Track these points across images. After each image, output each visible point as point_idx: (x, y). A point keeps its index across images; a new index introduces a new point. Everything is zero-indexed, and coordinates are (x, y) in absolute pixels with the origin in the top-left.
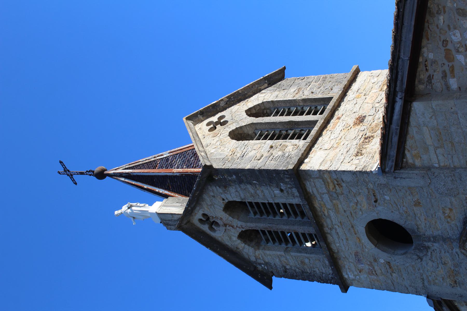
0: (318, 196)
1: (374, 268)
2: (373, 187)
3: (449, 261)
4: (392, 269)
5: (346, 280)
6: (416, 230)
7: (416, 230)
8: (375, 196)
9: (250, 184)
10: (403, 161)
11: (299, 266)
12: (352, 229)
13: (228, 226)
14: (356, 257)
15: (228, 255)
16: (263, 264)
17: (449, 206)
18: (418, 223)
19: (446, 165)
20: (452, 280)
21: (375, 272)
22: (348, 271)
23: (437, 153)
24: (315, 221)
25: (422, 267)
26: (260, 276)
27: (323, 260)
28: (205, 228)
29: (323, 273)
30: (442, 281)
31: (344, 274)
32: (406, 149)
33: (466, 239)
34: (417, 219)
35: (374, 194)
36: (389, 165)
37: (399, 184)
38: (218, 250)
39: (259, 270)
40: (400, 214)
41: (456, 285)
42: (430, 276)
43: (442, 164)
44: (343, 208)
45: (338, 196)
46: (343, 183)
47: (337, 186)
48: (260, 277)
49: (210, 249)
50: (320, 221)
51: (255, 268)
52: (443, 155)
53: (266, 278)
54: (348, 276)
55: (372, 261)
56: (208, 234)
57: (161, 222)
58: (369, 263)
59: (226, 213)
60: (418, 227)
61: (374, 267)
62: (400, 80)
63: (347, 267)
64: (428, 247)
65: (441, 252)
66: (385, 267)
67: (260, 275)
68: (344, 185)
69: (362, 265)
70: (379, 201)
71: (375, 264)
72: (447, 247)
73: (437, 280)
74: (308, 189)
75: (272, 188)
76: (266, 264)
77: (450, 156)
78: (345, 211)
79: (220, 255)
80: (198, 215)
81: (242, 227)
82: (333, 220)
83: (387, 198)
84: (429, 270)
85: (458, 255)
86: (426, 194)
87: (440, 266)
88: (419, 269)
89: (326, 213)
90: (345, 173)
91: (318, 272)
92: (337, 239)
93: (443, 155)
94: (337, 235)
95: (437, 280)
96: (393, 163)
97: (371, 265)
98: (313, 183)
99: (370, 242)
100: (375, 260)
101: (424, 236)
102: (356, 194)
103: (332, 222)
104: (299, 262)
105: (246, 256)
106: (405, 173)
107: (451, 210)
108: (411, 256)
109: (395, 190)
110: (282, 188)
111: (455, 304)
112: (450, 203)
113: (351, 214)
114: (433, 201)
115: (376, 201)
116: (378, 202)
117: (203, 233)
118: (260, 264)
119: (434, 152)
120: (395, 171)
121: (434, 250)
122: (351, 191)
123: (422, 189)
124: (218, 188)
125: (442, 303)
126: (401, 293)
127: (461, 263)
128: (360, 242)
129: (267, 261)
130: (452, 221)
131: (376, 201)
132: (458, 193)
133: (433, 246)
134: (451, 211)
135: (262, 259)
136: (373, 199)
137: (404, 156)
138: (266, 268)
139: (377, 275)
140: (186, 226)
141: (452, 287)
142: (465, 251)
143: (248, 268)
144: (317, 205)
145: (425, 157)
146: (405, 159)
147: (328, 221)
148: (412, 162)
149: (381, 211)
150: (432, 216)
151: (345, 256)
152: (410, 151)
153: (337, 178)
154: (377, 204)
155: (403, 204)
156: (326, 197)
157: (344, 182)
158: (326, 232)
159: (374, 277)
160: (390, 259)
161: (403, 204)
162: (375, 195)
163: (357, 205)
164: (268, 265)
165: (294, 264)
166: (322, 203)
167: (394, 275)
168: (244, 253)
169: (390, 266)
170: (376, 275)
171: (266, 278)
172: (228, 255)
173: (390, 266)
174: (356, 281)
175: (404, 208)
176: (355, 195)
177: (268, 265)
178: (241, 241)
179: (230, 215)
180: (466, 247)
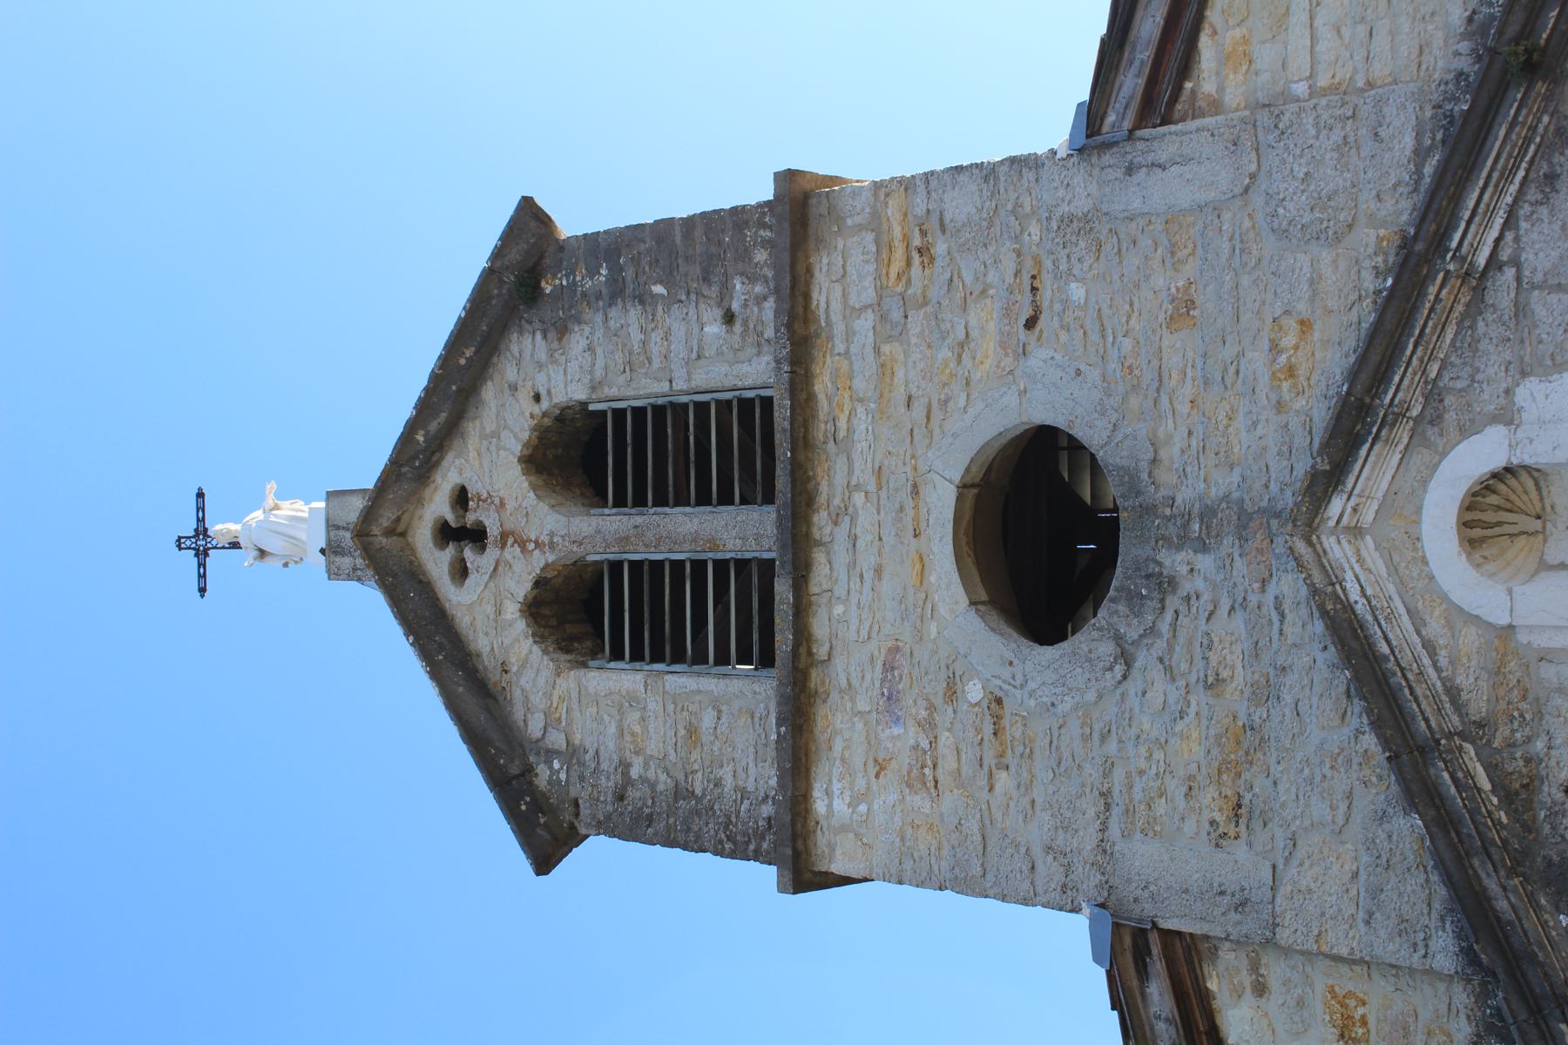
0: (839, 329)
1: (934, 742)
2: (1038, 237)
3: (1239, 670)
4: (1001, 744)
5: (815, 831)
6: (1145, 476)
7: (1145, 476)
8: (1037, 289)
9: (642, 302)
10: (1178, 89)
11: (672, 756)
12: (909, 503)
13: (510, 541)
14: (883, 681)
15: (461, 689)
16: (558, 753)
17: (1302, 307)
18: (1161, 433)
19: (1337, 80)
20: (1226, 797)
21: (935, 766)
22: (837, 770)
23: (1315, 25)
24: (789, 454)
25: (1123, 713)
26: (526, 803)
27: (765, 709)
28: (436, 562)
29: (744, 794)
30: (1181, 804)
31: (817, 792)
32: (1206, 26)
33: (1328, 468)
34: (1164, 399)
35: (1034, 277)
36: (1121, 95)
37: (1136, 204)
38: (441, 657)
39: (537, 787)
40: (1105, 385)
41: (1237, 825)
42: (1141, 773)
43: (1323, 81)
44: (907, 383)
45: (906, 317)
46: (939, 233)
47: (916, 255)
48: (523, 807)
49: (412, 645)
50: (811, 474)
51: (529, 770)
52: (1339, 32)
53: (542, 821)
54: (830, 806)
55: (938, 701)
56: (438, 599)
57: (323, 551)
58: (923, 713)
59: (526, 472)
60: (1156, 452)
61: (936, 737)
62: (1356, 602)
63: (838, 746)
64: (1169, 583)
65: (1215, 607)
66: (978, 730)
67: (528, 799)
68: (940, 248)
69: (897, 731)
70: (1042, 323)
71: (945, 716)
72: (1245, 572)
73: (1163, 800)
74: (815, 295)
75: (702, 306)
76: (572, 754)
77: (1362, 30)
78: (910, 398)
79: (435, 674)
80: (438, 505)
81: (552, 545)
82: (858, 465)
83: (1077, 292)
84: (1144, 736)
85: (1282, 616)
86: (1226, 246)
87: (1198, 699)
88: (1106, 730)
89: (842, 424)
90: (963, 178)
91: (729, 782)
92: (843, 576)
93: (1339, 32)
94: (850, 551)
95: (1163, 800)
96: (1140, 81)
97: (928, 726)
98: (840, 258)
99: (955, 576)
100: (952, 692)
101: (1168, 512)
102: (971, 293)
103: (851, 471)
104: (682, 732)
105: (518, 713)
106: (1170, 133)
107: (1305, 325)
108: (1093, 645)
109: (1116, 246)
110: (736, 306)
111: (1209, 985)
112: (1312, 282)
113: (928, 417)
114: (1245, 281)
115: (1031, 324)
116: (1037, 330)
117: (426, 587)
118: (550, 754)
119: (1305, 17)
120: (1139, 133)
121: (1188, 599)
122: (959, 276)
123: (1219, 216)
124: (539, 336)
125: (1150, 953)
126: (1004, 898)
127: (1284, 669)
128: (921, 583)
129: (577, 740)
130: (1298, 394)
131: (1031, 324)
132: (1350, 220)
133: (1192, 570)
134: (1304, 332)
135: (564, 724)
136: (1027, 313)
137: (1187, 65)
138: (563, 776)
139: (936, 787)
140: (384, 540)
141: (1217, 845)
142: (1310, 550)
143: (502, 761)
144: (822, 385)
145: (1266, 56)
146: (1189, 81)
147: (840, 465)
148: (1214, 93)
149: (1039, 376)
150: (1223, 378)
151: (849, 684)
152: (1219, 31)
153: (928, 210)
154: (1031, 337)
155: (1127, 322)
156: (865, 325)
157: (943, 231)
158: (817, 537)
159: (920, 802)
160: (1006, 673)
161: (1127, 322)
162: (1039, 286)
163: (959, 362)
164: (574, 761)
165: (661, 745)
166: (845, 365)
167: (1003, 780)
168: (517, 693)
169: (997, 719)
170: (933, 790)
171: (542, 821)
172: (461, 689)
173: (997, 719)
174: (851, 835)
175: (1127, 344)
176: (965, 298)
177: (574, 761)
178: (528, 625)
179: (534, 487)
180: (1318, 537)
